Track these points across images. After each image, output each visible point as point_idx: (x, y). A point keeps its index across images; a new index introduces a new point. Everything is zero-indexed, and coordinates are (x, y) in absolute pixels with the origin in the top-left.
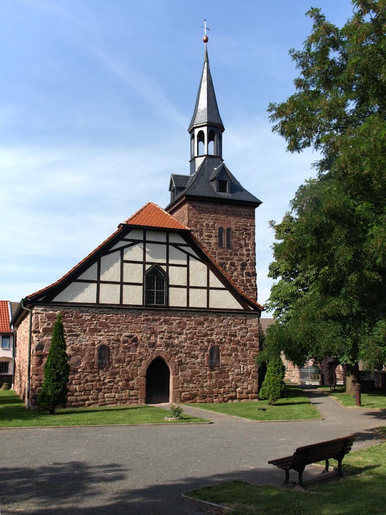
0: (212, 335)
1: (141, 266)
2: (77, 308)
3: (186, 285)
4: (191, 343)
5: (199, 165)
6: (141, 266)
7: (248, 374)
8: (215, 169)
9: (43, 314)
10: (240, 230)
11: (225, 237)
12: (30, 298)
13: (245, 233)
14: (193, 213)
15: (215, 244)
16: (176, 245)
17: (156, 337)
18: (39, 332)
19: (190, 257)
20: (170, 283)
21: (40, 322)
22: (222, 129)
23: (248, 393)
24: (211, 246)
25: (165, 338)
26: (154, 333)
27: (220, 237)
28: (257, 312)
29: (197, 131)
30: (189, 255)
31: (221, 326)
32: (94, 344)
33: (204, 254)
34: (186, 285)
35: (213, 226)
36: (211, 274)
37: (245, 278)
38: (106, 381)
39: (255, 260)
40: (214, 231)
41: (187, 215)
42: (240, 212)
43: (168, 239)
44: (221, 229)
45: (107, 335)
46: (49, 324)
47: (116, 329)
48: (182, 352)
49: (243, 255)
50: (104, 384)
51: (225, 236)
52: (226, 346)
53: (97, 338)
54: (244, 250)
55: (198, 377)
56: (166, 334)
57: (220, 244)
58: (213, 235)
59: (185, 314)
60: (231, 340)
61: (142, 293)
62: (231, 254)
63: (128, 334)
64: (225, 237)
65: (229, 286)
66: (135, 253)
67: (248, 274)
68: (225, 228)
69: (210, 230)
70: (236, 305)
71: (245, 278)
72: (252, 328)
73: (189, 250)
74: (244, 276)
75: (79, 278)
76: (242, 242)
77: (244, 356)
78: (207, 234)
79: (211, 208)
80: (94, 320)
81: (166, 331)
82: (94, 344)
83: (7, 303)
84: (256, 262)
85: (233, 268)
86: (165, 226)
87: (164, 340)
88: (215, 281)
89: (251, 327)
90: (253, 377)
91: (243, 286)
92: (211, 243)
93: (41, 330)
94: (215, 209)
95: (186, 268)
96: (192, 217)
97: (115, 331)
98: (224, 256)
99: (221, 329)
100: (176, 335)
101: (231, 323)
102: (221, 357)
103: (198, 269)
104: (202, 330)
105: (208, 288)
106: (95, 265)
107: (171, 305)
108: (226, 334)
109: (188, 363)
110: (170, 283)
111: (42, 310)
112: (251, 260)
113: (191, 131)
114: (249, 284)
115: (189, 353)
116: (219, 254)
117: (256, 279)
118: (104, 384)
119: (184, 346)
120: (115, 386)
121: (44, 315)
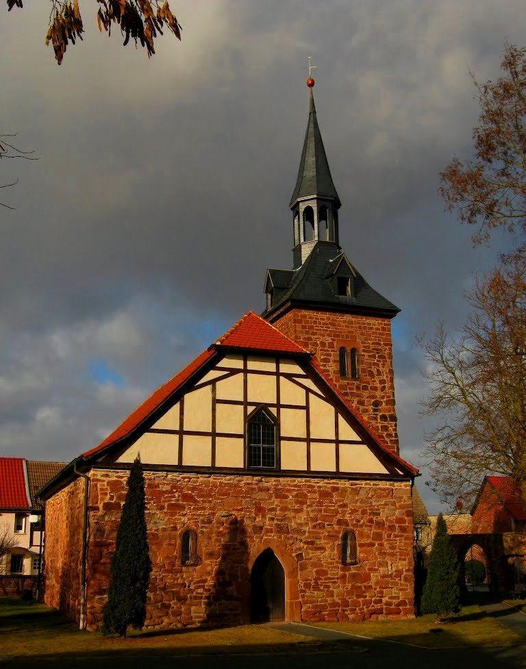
0: (344, 513)
1: (241, 407)
3: (305, 437)
4: (314, 527)
5: (307, 256)
7: (399, 573)
8: (331, 261)
9: (104, 481)
10: (371, 352)
11: (348, 361)
12: (86, 457)
14: (302, 326)
16: (289, 377)
17: (264, 516)
18: (97, 509)
19: (310, 394)
20: (283, 434)
22: (337, 204)
23: (398, 605)
25: (277, 520)
26: (260, 510)
27: (342, 362)
29: (302, 207)
30: (308, 390)
31: (357, 501)
33: (330, 389)
34: (305, 437)
35: (331, 345)
37: (380, 425)
38: (192, 588)
39: (394, 396)
41: (292, 330)
42: (369, 324)
43: (278, 368)
44: (342, 350)
46: (112, 498)
47: (207, 505)
48: (301, 541)
49: (376, 389)
51: (348, 358)
52: (366, 530)
53: (181, 519)
54: (377, 382)
55: (325, 579)
56: (278, 512)
57: (342, 372)
58: (332, 358)
59: (306, 481)
60: (371, 521)
61: (243, 449)
62: (358, 388)
63: (224, 513)
64: (348, 361)
65: (367, 439)
66: (230, 388)
67: (384, 418)
68: (348, 349)
69: (326, 351)
71: (380, 425)
72: (402, 503)
73: (308, 383)
74: (379, 421)
75: (153, 427)
76: (374, 371)
77: (393, 548)
78: (322, 357)
81: (278, 508)
82: (175, 529)
83: (5, 462)
85: (361, 407)
86: (242, 346)
87: (276, 522)
88: (347, 432)
89: (400, 501)
90: (406, 579)
92: (328, 371)
93: (101, 506)
95: (304, 412)
96: (301, 332)
97: (204, 508)
98: (348, 391)
99: (358, 504)
100: (293, 514)
101: (373, 496)
102: (358, 548)
103: (323, 412)
104: (330, 506)
105: (337, 442)
106: (176, 407)
107: (283, 468)
108: (364, 512)
109: (311, 559)
110: (283, 434)
111: (102, 476)
112: (388, 397)
113: (295, 208)
114: (385, 433)
115: (312, 543)
117: (396, 425)
119: (305, 532)
121: (105, 483)
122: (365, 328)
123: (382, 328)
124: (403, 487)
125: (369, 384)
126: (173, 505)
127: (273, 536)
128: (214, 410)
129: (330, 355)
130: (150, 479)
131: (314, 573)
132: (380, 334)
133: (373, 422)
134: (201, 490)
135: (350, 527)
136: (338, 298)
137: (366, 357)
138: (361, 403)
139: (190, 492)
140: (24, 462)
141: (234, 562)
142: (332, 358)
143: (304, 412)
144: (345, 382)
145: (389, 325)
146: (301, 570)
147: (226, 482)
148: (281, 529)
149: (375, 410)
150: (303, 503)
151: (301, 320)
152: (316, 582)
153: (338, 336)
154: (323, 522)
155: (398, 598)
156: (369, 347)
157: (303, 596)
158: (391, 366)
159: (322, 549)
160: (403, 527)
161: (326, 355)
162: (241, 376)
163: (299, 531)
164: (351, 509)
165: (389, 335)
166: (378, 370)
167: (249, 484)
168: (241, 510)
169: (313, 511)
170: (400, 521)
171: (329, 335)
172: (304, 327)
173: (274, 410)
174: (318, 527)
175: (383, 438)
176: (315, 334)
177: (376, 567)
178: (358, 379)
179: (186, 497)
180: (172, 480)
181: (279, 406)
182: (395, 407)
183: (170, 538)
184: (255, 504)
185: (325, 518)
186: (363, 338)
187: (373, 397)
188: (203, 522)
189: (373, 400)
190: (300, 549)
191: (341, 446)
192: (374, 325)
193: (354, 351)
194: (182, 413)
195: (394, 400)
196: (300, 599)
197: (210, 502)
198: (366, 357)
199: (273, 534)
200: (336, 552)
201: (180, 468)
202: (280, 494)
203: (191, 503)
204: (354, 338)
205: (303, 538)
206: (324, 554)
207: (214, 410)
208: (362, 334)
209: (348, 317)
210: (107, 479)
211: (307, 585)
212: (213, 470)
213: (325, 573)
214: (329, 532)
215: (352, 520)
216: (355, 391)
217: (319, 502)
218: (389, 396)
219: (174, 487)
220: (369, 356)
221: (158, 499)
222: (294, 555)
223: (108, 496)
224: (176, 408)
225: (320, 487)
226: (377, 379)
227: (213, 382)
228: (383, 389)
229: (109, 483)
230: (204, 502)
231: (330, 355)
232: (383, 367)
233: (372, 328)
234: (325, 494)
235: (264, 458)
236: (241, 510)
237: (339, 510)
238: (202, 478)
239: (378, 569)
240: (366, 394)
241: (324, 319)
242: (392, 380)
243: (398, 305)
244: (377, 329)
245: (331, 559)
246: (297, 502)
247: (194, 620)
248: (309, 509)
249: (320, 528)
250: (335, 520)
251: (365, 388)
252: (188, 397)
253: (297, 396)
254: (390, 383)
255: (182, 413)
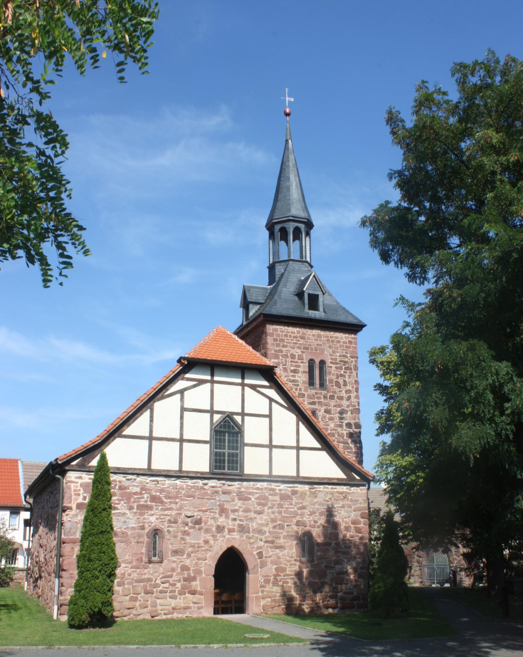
0: (302, 515)
2: (122, 475)
4: (274, 527)
6: (208, 415)
9: (77, 483)
13: (343, 367)
15: (304, 382)
16: (253, 387)
19: (273, 404)
21: (73, 494)
24: (298, 385)
25: (240, 520)
26: (223, 511)
28: (365, 483)
29: (277, 228)
30: (271, 400)
32: (143, 528)
36: (302, 427)
39: (359, 405)
40: (302, 364)
42: (337, 338)
44: (311, 362)
45: (162, 515)
47: (174, 506)
49: (341, 398)
50: (156, 586)
54: (344, 392)
55: (284, 576)
57: (311, 383)
58: (301, 369)
62: (325, 397)
68: (317, 361)
70: (337, 473)
71: (345, 432)
72: (358, 505)
73: (272, 393)
78: (292, 368)
79: (298, 332)
80: (144, 492)
81: (241, 510)
82: (143, 528)
84: (361, 409)
85: (328, 416)
87: (238, 522)
91: (343, 443)
92: (297, 381)
94: (303, 334)
95: (267, 420)
98: (316, 400)
102: (316, 547)
109: (270, 557)
115: (272, 542)
116: (310, 397)
118: (156, 586)
119: (265, 532)
120: (171, 588)
121: (79, 485)
122: (333, 341)
123: (349, 341)
124: (359, 491)
125: (336, 394)
126: (142, 505)
127: (236, 535)
128: (182, 417)
129: (299, 366)
130: (120, 482)
131: (274, 570)
132: (346, 347)
133: (339, 429)
134: (169, 492)
135: (308, 528)
136: (308, 313)
137: (333, 369)
138: (327, 411)
139: (158, 494)
140: (19, 461)
141: (198, 559)
142: (301, 369)
143: (267, 420)
144: (314, 391)
145: (356, 339)
146: (261, 568)
147: (193, 485)
148: (243, 529)
149: (341, 418)
150: (264, 505)
151: (273, 334)
152: (275, 578)
153: (307, 349)
154: (283, 523)
155: (352, 593)
156: (336, 360)
157: (263, 592)
158: (357, 377)
159: (281, 547)
160: (359, 528)
161: (296, 366)
162: (209, 385)
163: (260, 532)
164: (310, 511)
165: (355, 348)
166: (345, 381)
167: (213, 487)
168: (206, 511)
169: (273, 513)
170: (354, 522)
171: (299, 348)
172: (275, 340)
173: (238, 419)
174: (278, 527)
175: (348, 444)
176: (286, 346)
177: (333, 565)
178: (325, 389)
179: (154, 499)
180: (141, 482)
181: (243, 414)
182: (360, 415)
183: (140, 536)
184: (219, 506)
185: (284, 519)
186: (331, 351)
187: (340, 406)
188: (169, 521)
189: (339, 409)
190: (260, 548)
191: (301, 452)
192: (341, 338)
193: (322, 363)
194: (152, 420)
195: (359, 409)
196: (260, 594)
197: (176, 503)
198: (333, 369)
199: (235, 534)
200: (294, 550)
201: (150, 473)
202: (242, 497)
203: (158, 504)
204: (322, 351)
205: (263, 537)
206: (283, 552)
207: (182, 417)
208: (330, 347)
209: (316, 332)
210: (80, 481)
211: (267, 581)
212: (180, 475)
213: (284, 570)
214: (288, 532)
215: (310, 521)
216: (322, 400)
217: (279, 505)
218: (355, 406)
219: (142, 489)
220: (336, 368)
221: (129, 499)
222: (255, 553)
223: (81, 497)
224: (146, 414)
225: (280, 490)
226: (343, 389)
227: (182, 392)
228: (349, 398)
229: (81, 485)
230: (171, 503)
231: (299, 366)
232: (349, 378)
233: (339, 342)
234: (284, 497)
235: (229, 462)
236: (206, 511)
237: (299, 511)
238: (168, 482)
239: (334, 567)
240: (333, 403)
241: (294, 333)
242: (357, 390)
243: (364, 321)
244: (344, 342)
245: (290, 557)
246: (259, 504)
247: (159, 612)
248: (270, 510)
249: (280, 529)
250: (295, 520)
251: (332, 397)
252: (158, 405)
253: (262, 405)
254: (355, 393)
255: (152, 420)
